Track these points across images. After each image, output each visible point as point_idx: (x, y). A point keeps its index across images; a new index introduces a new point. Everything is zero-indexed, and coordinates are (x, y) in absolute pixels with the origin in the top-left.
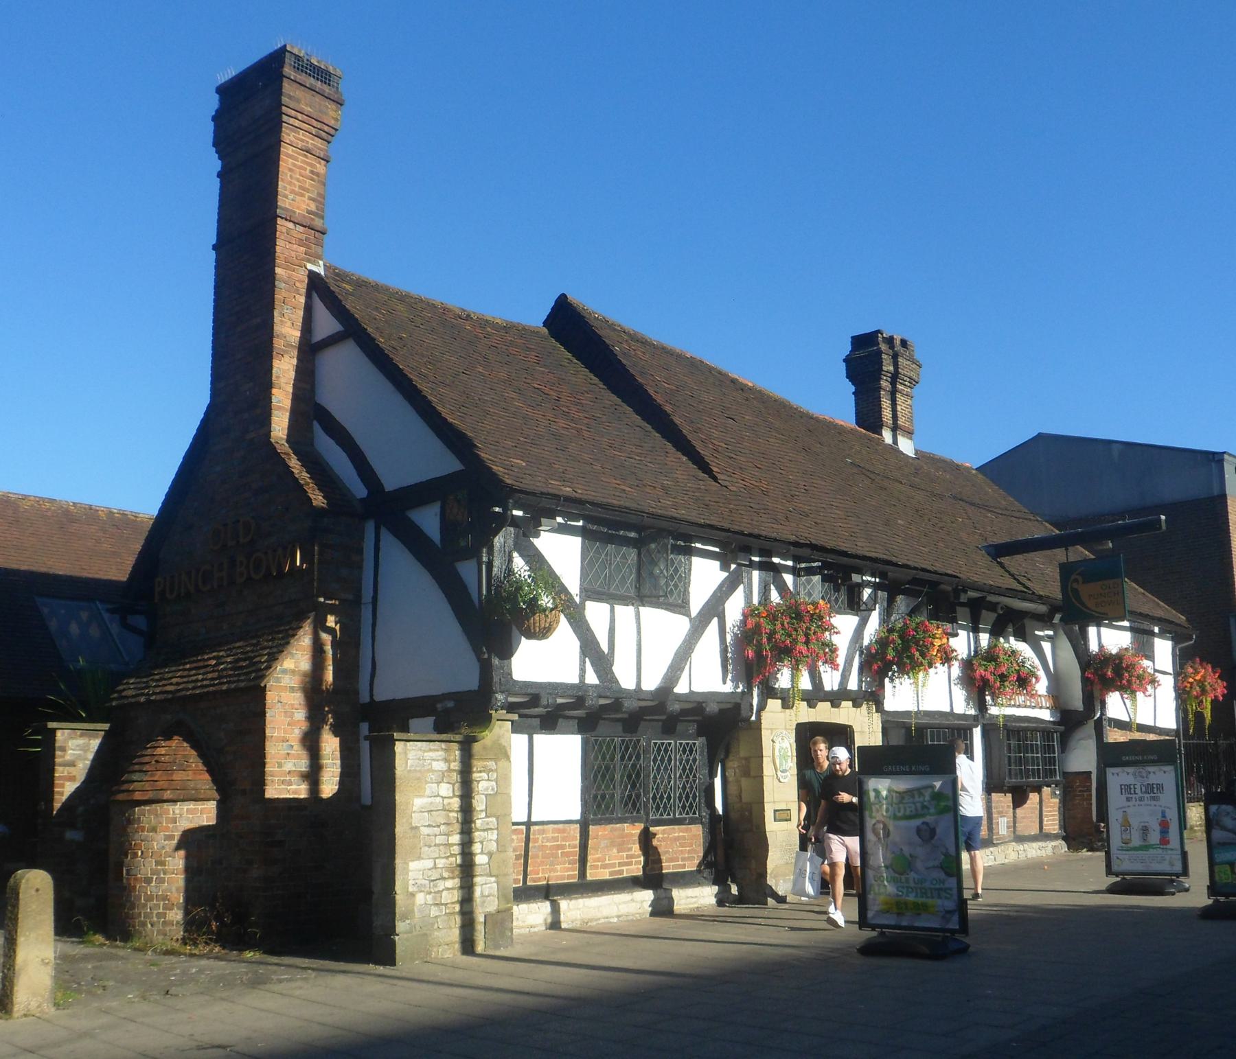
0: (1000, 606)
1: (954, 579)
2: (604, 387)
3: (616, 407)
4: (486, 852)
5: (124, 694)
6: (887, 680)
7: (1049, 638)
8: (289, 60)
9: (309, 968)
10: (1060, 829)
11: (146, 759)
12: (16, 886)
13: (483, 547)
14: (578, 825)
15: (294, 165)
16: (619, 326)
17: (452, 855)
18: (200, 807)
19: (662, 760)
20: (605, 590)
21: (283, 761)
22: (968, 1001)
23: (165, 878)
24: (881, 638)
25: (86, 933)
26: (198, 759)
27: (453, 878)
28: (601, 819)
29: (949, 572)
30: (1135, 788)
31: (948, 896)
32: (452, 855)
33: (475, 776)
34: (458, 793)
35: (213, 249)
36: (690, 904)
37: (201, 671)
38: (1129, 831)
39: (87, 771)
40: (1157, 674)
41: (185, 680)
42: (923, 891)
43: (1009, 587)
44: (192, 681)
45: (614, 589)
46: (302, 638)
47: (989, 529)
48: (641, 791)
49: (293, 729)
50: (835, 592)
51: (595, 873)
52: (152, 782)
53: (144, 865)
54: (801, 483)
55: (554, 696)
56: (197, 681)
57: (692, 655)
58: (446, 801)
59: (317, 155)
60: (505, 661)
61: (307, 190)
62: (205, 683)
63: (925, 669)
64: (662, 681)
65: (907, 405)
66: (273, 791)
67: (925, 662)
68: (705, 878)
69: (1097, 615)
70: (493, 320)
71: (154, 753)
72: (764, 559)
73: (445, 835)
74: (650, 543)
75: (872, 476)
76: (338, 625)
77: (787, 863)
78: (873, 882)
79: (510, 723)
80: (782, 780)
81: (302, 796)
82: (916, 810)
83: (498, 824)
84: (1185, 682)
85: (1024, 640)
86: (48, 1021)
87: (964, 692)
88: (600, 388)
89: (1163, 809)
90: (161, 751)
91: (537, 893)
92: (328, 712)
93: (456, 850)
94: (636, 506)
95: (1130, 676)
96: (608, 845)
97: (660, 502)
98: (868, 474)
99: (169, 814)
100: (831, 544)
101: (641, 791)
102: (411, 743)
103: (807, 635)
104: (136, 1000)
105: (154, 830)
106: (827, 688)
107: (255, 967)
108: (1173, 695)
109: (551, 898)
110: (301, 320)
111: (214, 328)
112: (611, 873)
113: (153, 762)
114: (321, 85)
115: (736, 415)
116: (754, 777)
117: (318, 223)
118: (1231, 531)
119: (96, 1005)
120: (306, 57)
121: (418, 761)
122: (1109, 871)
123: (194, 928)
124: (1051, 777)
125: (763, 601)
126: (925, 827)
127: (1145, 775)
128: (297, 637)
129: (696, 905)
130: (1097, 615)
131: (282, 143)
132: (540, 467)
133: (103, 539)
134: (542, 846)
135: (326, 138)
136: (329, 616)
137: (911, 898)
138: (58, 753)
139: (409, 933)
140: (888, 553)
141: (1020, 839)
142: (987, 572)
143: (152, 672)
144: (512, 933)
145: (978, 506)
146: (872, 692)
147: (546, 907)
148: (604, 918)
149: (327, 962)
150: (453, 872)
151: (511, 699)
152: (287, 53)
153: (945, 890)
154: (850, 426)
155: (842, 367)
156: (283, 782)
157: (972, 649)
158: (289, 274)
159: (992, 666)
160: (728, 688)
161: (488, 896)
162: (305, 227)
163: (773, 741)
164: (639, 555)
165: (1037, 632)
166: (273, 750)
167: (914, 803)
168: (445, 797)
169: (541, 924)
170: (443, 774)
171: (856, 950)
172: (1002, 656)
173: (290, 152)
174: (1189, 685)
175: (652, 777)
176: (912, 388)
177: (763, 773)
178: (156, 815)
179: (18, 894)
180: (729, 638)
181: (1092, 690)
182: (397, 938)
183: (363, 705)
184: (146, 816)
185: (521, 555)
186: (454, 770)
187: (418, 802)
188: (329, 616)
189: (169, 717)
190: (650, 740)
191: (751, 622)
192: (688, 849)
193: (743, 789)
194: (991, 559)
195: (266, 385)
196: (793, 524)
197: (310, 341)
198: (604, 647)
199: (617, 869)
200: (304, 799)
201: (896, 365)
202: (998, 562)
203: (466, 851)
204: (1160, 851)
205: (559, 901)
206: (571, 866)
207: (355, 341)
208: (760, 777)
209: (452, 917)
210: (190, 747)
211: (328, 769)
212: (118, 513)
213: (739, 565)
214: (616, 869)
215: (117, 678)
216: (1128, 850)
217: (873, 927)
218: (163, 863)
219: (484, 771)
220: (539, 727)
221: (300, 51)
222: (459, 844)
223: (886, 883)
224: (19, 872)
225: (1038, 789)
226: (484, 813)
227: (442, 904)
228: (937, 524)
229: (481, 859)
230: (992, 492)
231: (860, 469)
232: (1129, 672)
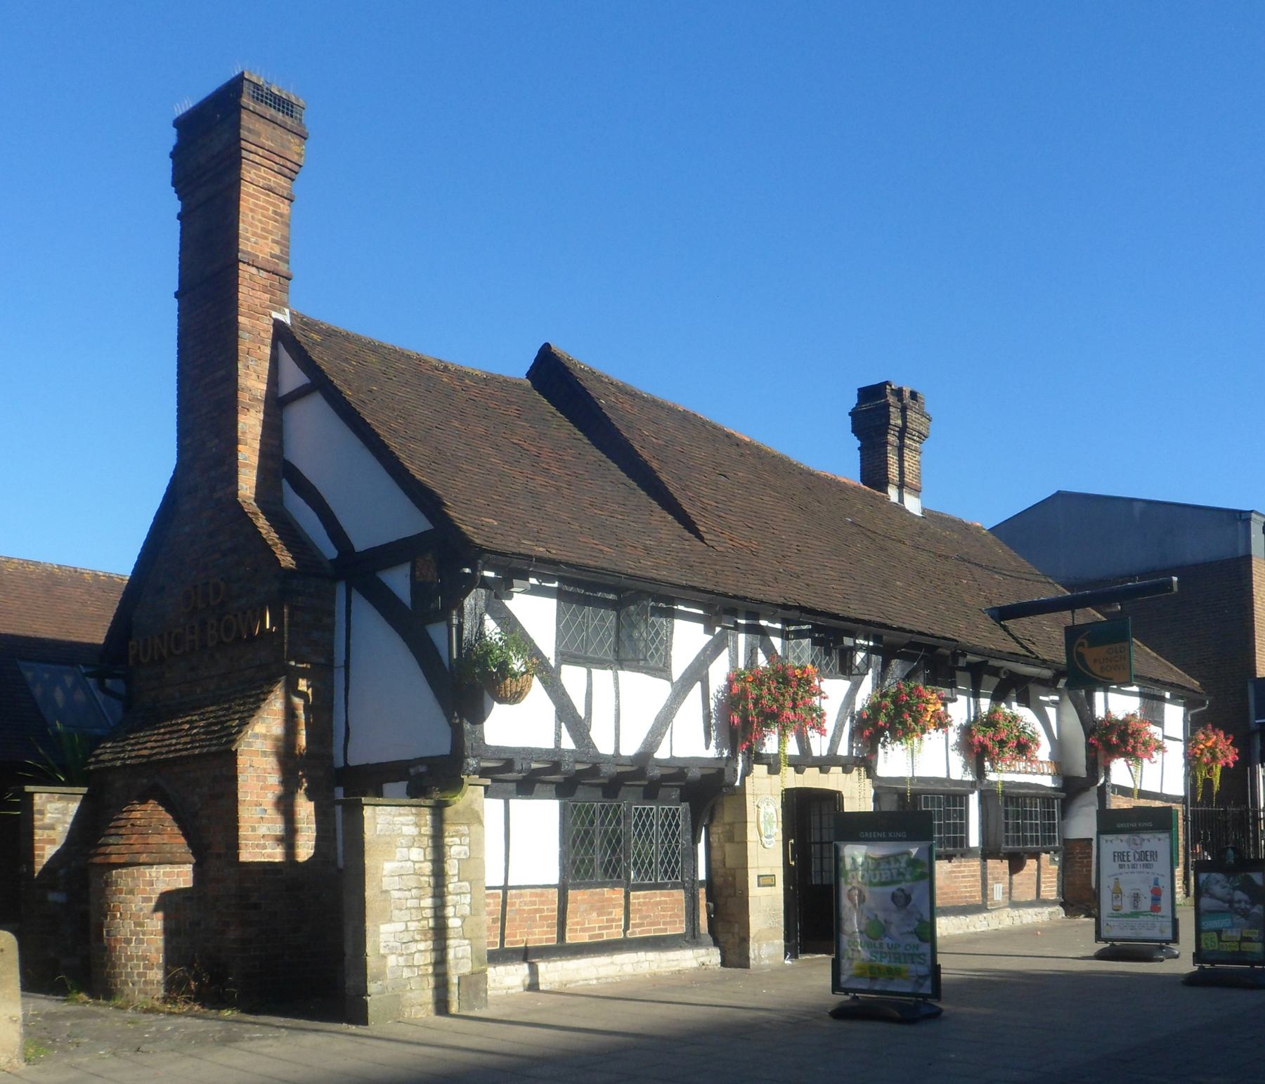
0: (1002, 671)
1: (951, 642)
2: (588, 442)
3: (601, 463)
5: (101, 758)
7: (1054, 703)
8: (247, 89)
9: (283, 1027)
10: (1058, 895)
11: (122, 823)
15: (256, 205)
16: (607, 377)
17: (427, 918)
18: (176, 870)
19: (644, 825)
21: (257, 825)
24: (874, 703)
25: (70, 992)
26: (174, 824)
27: (426, 941)
28: (581, 884)
30: (1128, 856)
33: (447, 840)
34: (429, 857)
35: (176, 297)
37: (175, 736)
40: (1165, 740)
41: (159, 744)
42: (897, 956)
43: (1012, 651)
44: (167, 746)
46: (273, 703)
47: (995, 590)
48: (622, 856)
54: (793, 542)
56: (171, 745)
57: (674, 720)
58: (417, 865)
61: (270, 232)
62: (178, 747)
63: (917, 736)
64: (641, 747)
66: (247, 854)
67: (918, 728)
68: (687, 942)
69: (1101, 679)
70: (472, 372)
72: (750, 622)
73: (416, 898)
74: (630, 605)
75: (872, 535)
76: (310, 689)
78: (847, 947)
80: (766, 846)
81: (277, 860)
82: (892, 876)
85: (1028, 706)
86: (17, 1076)
87: (962, 758)
91: (514, 956)
92: (303, 776)
95: (1135, 743)
98: (868, 533)
100: (821, 605)
101: (622, 856)
102: (380, 807)
103: (794, 700)
104: (107, 1056)
105: (131, 892)
106: (816, 753)
107: (230, 1025)
108: (1182, 761)
110: (267, 373)
111: (178, 381)
112: (590, 937)
113: (129, 826)
116: (738, 843)
117: (283, 268)
119: (66, 1061)
120: (266, 85)
122: (1098, 937)
123: (174, 987)
125: (749, 666)
126: (901, 893)
128: (267, 701)
130: (1101, 679)
132: (512, 526)
135: (289, 176)
136: (300, 680)
137: (885, 963)
138: (36, 816)
139: (380, 994)
140: (882, 616)
141: (1015, 905)
142: (989, 635)
143: (128, 736)
145: (987, 568)
146: (863, 758)
148: (584, 980)
149: (302, 1021)
150: (425, 935)
151: (484, 764)
152: (245, 81)
154: (852, 482)
155: (848, 420)
156: (257, 846)
157: (972, 714)
159: (991, 732)
160: (712, 753)
161: (462, 958)
162: (269, 272)
163: (758, 807)
164: (618, 618)
165: (1041, 698)
167: (890, 870)
168: (417, 862)
169: (519, 986)
172: (1001, 722)
173: (251, 191)
174: (1199, 752)
177: (746, 838)
178: (133, 878)
180: (712, 705)
181: (1096, 756)
182: (369, 998)
183: (339, 771)
184: (122, 878)
185: (493, 618)
186: (425, 835)
187: (388, 867)
188: (300, 680)
189: (145, 781)
190: (631, 804)
191: (737, 687)
193: (727, 855)
194: (993, 622)
195: (231, 441)
196: (781, 586)
197: (277, 394)
198: (581, 711)
199: (597, 932)
200: (279, 862)
201: (904, 418)
202: (1001, 625)
203: (439, 914)
204: (1150, 918)
207: (322, 394)
208: (744, 843)
209: (425, 979)
215: (97, 741)
216: (1116, 917)
218: (141, 925)
219: (456, 836)
220: (515, 792)
221: (259, 79)
222: (431, 908)
223: (860, 948)
225: (1036, 856)
227: (415, 966)
228: (938, 586)
229: (453, 923)
230: (1001, 551)
231: (861, 529)
232: (1135, 738)
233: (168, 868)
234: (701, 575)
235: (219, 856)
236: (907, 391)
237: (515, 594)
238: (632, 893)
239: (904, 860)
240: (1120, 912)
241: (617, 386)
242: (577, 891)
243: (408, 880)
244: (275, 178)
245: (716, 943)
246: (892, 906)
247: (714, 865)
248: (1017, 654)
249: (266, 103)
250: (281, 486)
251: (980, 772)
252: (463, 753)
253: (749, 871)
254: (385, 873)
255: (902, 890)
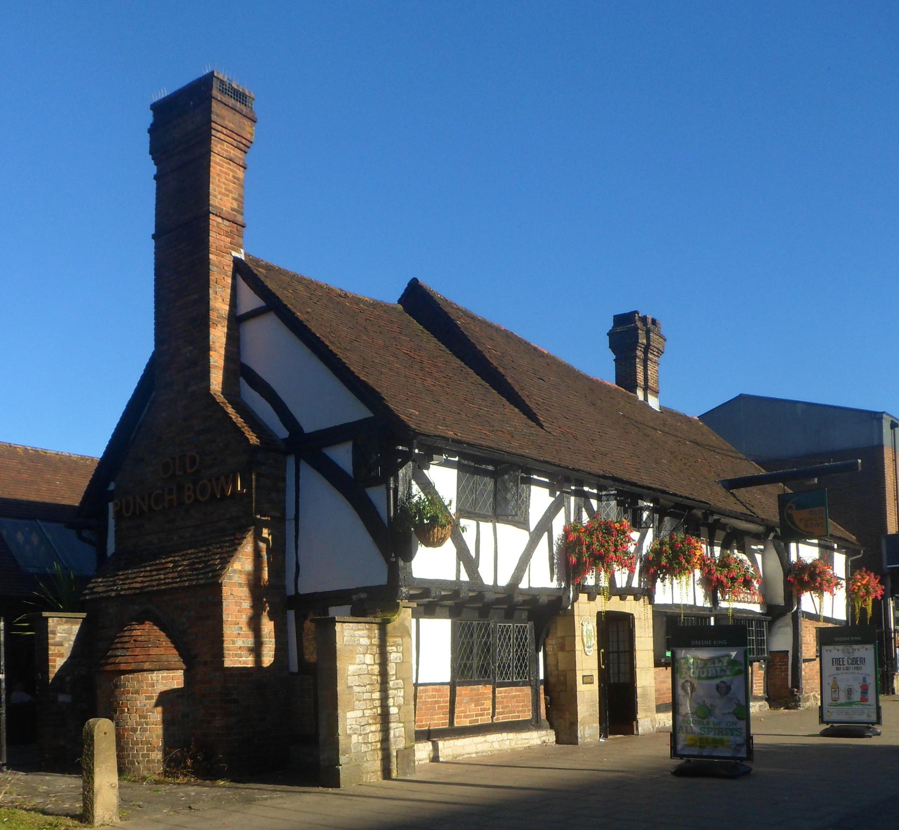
2: (449, 352)
3: (462, 369)
4: (396, 705)
5: (95, 590)
6: (659, 580)
8: (216, 84)
10: (764, 693)
11: (126, 639)
12: (91, 731)
13: (391, 476)
14: (449, 686)
15: (221, 171)
17: (375, 707)
18: (171, 675)
20: (473, 510)
21: (235, 639)
22: (776, 804)
23: (147, 728)
26: (167, 639)
27: (376, 724)
28: (464, 682)
29: (703, 500)
30: (843, 661)
31: (739, 734)
32: (375, 707)
33: (389, 648)
34: (377, 661)
36: (524, 744)
37: (162, 572)
38: (837, 692)
39: (71, 649)
45: (478, 510)
48: (491, 661)
49: (242, 615)
50: (624, 514)
51: (460, 722)
52: (134, 656)
53: (130, 719)
55: (440, 590)
58: (370, 667)
59: (238, 163)
60: (408, 563)
62: (167, 581)
64: (511, 579)
65: (655, 370)
68: (533, 725)
70: (363, 298)
71: (132, 634)
72: (579, 488)
73: (369, 692)
76: (271, 536)
77: (591, 714)
79: (410, 609)
80: (588, 654)
81: (249, 666)
83: (404, 684)
84: (854, 586)
87: (703, 590)
88: (447, 353)
89: (865, 676)
90: (137, 633)
92: (266, 602)
93: (377, 703)
94: (497, 446)
96: (469, 701)
97: (511, 443)
99: (149, 680)
100: (626, 477)
101: (491, 661)
102: (346, 624)
103: (616, 546)
105: (137, 692)
106: (619, 586)
109: (431, 740)
113: (132, 641)
114: (240, 105)
115: (544, 377)
116: (569, 651)
117: (239, 218)
118: (886, 473)
120: (228, 82)
121: (350, 638)
122: (822, 720)
124: (762, 655)
127: (851, 651)
128: (242, 545)
129: (528, 745)
130: (805, 534)
131: (212, 153)
133: (22, 470)
134: (425, 701)
136: (264, 529)
137: (711, 735)
138: (50, 636)
139: (347, 764)
143: (118, 573)
144: (414, 764)
147: (429, 746)
148: (467, 754)
151: (411, 592)
152: (214, 78)
153: (737, 730)
155: (607, 339)
156: (236, 655)
158: (219, 259)
159: (726, 571)
160: (554, 585)
163: (582, 625)
165: (753, 547)
166: (229, 631)
167: (715, 668)
168: (369, 665)
170: (367, 647)
171: (670, 773)
173: (218, 160)
175: (497, 651)
176: (658, 357)
177: (575, 648)
178: (138, 681)
179: (93, 736)
182: (340, 767)
183: (290, 597)
184: (130, 682)
185: (417, 483)
186: (375, 645)
187: (352, 668)
188: (264, 529)
190: (496, 623)
191: (574, 535)
192: (521, 704)
195: (205, 348)
198: (473, 553)
199: (475, 718)
200: (251, 667)
201: (648, 338)
203: (384, 704)
204: (861, 707)
205: (438, 742)
206: (443, 716)
208: (573, 651)
209: (375, 752)
210: (160, 629)
211: (267, 645)
212: (31, 450)
213: (562, 492)
214: (474, 719)
216: (836, 706)
217: (681, 757)
218: (145, 717)
222: (379, 699)
224: (90, 720)
226: (395, 676)
227: (369, 743)
229: (393, 710)
233: (165, 674)
234: (549, 453)
235: (205, 663)
236: (650, 317)
237: (431, 465)
238: (497, 689)
239: (725, 660)
240: (838, 702)
241: (462, 311)
242: (462, 687)
243: (365, 678)
244: (234, 150)
245: (552, 727)
246: (716, 694)
247: (549, 668)
248: (746, 514)
249: (228, 95)
250: (239, 382)
251: (715, 601)
252: (398, 583)
253: (577, 672)
254: (349, 673)
255: (724, 682)
